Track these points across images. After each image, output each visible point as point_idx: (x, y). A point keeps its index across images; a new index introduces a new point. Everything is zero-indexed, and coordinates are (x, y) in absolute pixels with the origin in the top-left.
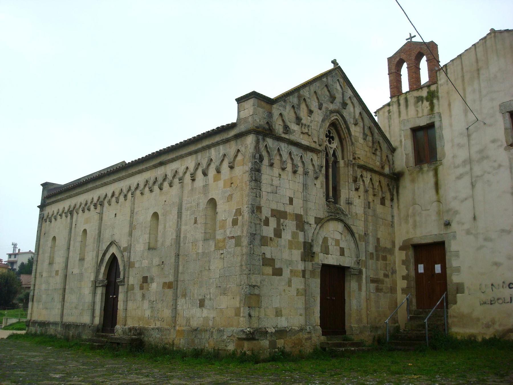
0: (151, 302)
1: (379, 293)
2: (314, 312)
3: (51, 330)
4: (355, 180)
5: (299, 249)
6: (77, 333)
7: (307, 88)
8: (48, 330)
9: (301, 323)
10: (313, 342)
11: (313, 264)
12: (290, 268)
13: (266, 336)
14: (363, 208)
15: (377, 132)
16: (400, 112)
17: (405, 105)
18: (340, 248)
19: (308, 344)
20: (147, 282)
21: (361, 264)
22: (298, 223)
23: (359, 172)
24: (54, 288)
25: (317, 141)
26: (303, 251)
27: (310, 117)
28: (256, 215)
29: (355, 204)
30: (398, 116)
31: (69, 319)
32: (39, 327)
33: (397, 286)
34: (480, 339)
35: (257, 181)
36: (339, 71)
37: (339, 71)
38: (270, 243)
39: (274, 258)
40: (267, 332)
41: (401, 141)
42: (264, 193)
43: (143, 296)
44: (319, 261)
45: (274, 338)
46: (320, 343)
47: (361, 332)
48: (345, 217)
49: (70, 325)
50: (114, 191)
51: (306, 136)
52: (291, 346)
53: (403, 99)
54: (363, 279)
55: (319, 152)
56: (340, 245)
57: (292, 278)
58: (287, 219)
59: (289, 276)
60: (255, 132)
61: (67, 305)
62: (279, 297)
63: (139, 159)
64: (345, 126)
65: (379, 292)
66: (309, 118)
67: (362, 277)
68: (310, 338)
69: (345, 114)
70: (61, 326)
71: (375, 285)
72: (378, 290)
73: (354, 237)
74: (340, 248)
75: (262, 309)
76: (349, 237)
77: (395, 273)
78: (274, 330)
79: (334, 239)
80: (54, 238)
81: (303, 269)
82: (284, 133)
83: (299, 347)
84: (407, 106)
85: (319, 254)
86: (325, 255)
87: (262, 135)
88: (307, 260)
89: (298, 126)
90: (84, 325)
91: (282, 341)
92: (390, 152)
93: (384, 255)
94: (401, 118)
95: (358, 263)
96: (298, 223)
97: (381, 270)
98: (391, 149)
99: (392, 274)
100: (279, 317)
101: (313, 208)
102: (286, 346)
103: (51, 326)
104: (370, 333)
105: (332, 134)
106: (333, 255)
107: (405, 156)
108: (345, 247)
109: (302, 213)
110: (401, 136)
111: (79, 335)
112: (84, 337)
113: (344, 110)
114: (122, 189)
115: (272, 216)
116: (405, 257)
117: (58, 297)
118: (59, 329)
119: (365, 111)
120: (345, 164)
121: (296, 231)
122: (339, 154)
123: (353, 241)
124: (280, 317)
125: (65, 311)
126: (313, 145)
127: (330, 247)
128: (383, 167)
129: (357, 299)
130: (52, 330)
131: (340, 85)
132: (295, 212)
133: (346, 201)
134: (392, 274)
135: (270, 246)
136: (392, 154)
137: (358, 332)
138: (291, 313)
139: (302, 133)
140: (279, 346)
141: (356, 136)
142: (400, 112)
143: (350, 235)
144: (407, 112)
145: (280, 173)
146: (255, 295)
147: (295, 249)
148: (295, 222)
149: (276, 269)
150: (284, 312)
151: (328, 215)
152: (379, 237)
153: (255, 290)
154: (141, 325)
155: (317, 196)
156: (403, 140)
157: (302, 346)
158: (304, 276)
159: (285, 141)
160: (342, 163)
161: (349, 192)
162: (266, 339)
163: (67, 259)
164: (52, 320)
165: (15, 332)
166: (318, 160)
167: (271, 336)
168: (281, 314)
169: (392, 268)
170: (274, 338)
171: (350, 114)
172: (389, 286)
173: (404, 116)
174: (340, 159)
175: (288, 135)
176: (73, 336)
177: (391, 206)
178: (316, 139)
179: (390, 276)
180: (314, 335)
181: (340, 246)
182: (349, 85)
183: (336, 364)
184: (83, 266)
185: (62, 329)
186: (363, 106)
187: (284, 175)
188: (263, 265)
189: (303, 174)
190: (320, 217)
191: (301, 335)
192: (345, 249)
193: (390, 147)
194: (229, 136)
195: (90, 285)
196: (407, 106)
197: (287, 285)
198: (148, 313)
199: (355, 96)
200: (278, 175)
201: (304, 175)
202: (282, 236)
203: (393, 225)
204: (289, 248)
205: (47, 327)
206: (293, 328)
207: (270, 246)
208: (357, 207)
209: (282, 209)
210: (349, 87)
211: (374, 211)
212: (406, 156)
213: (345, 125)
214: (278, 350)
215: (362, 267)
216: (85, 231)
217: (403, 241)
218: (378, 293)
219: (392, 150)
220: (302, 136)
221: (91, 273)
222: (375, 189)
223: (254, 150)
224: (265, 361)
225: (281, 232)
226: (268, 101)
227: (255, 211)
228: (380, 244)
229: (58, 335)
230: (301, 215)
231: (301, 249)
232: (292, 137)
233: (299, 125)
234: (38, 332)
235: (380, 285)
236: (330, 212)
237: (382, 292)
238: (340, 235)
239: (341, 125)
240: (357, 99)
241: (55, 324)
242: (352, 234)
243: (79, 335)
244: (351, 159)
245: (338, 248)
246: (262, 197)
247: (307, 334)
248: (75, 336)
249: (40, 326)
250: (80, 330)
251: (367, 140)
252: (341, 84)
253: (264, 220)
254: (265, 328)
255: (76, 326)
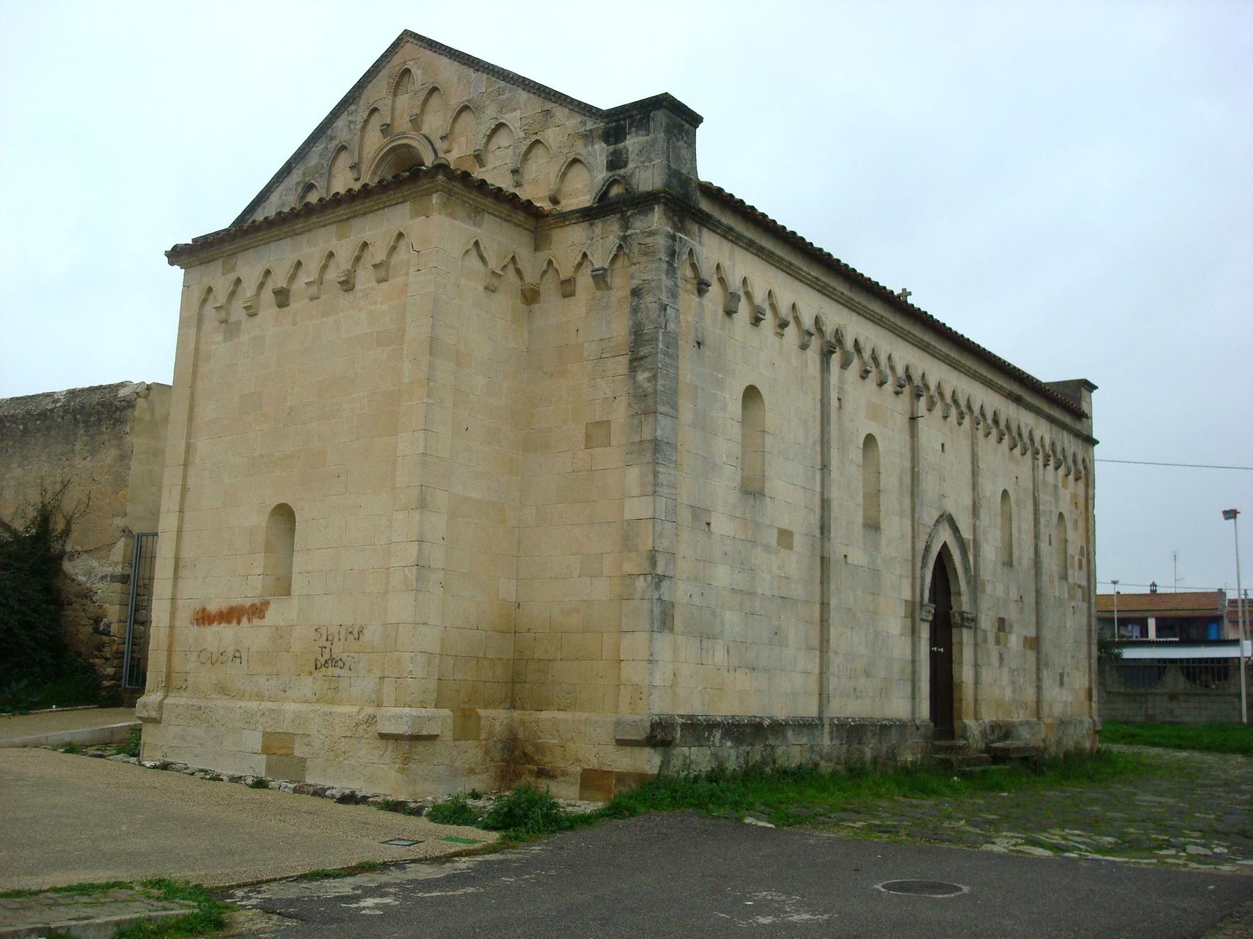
0: (1011, 671)
3: (792, 752)
6: (884, 749)
8: (779, 751)
20: (1004, 631)
24: (776, 593)
31: (848, 708)
32: (729, 744)
34: (767, 722)
43: (1001, 658)
49: (864, 725)
50: (856, 340)
61: (836, 661)
63: (846, 265)
70: (831, 733)
80: (751, 394)
90: (902, 726)
103: (790, 734)
111: (892, 755)
112: (908, 757)
114: (924, 374)
117: (797, 630)
118: (826, 741)
125: (833, 682)
130: (796, 751)
154: (1001, 718)
163: (825, 504)
164: (780, 713)
176: (875, 760)
183: (892, 772)
184: (876, 547)
185: (837, 742)
194: (757, 241)
195: (901, 611)
198: (1008, 693)
205: (771, 742)
216: (870, 439)
221: (901, 576)
229: (823, 764)
234: (732, 765)
241: (806, 726)
243: (892, 755)
248: (880, 757)
249: (738, 741)
250: (894, 737)
255: (884, 728)
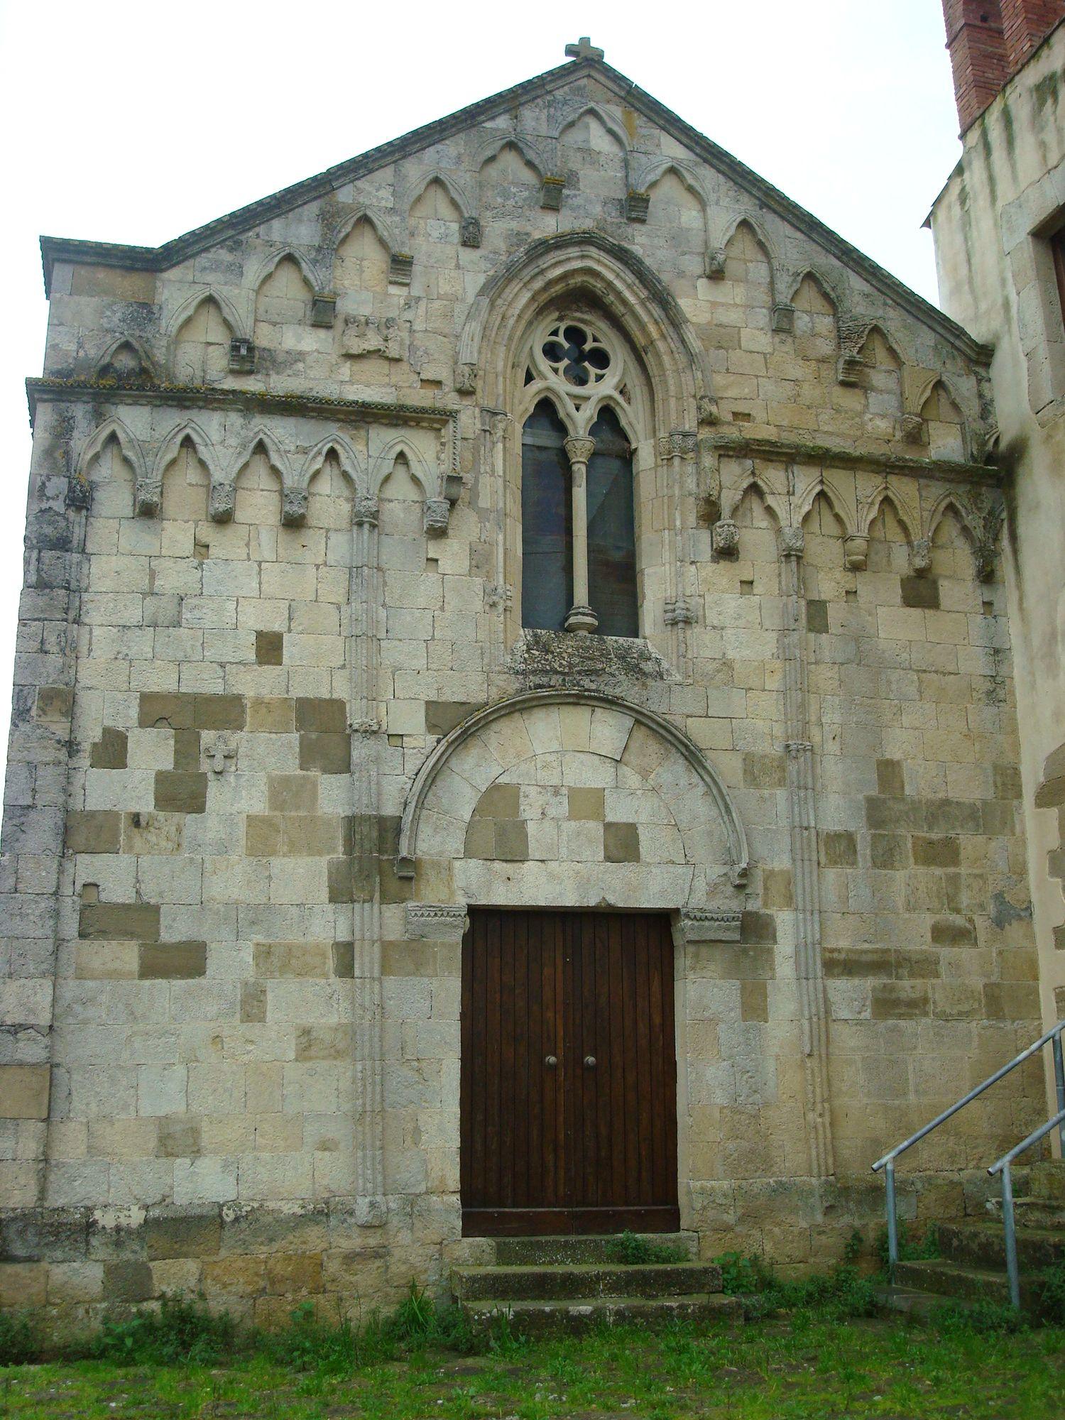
1: (902, 1023)
2: (417, 1131)
4: (710, 513)
5: (313, 851)
7: (386, 174)
9: (325, 1182)
10: (397, 1268)
11: (406, 911)
12: (259, 938)
13: (87, 1243)
14: (774, 635)
15: (866, 288)
16: (991, 180)
17: (1004, 145)
18: (608, 826)
19: (366, 1277)
21: (761, 891)
22: (314, 736)
23: (734, 477)
25: (443, 373)
26: (342, 857)
27: (407, 285)
28: (38, 727)
29: (712, 618)
30: (988, 204)
33: (1036, 978)
35: (52, 588)
36: (593, 73)
37: (593, 73)
38: (129, 838)
39: (153, 901)
40: (89, 1227)
41: (1006, 305)
42: (97, 632)
44: (452, 893)
45: (134, 1252)
46: (446, 1273)
47: (752, 1217)
48: (644, 684)
51: (373, 367)
52: (250, 1289)
53: (997, 120)
54: (778, 959)
55: (447, 421)
56: (607, 811)
57: (270, 984)
58: (240, 728)
59: (250, 974)
60: (44, 392)
62: (180, 1070)
64: (644, 294)
65: (900, 1016)
66: (393, 290)
67: (770, 952)
68: (380, 1253)
69: (640, 242)
71: (869, 983)
72: (887, 1005)
73: (703, 773)
74: (608, 826)
75: (72, 1125)
76: (674, 771)
77: (1020, 918)
78: (136, 1217)
79: (564, 791)
81: (343, 936)
82: (233, 372)
83: (304, 1292)
84: (1010, 142)
85: (457, 864)
86: (497, 865)
87: (85, 399)
88: (358, 895)
89: (322, 333)
91: (190, 1267)
92: (960, 362)
93: (935, 835)
94: (1000, 204)
95: (740, 887)
96: (314, 736)
97: (910, 908)
98: (968, 351)
99: (1000, 922)
100: (179, 1161)
101: (420, 663)
102: (211, 1288)
104: (819, 1218)
105: (595, 340)
106: (553, 865)
107: (1024, 363)
108: (642, 818)
109: (341, 692)
110: (1003, 282)
113: (637, 226)
115: (146, 721)
116: (1057, 834)
119: (775, 212)
120: (657, 453)
121: (299, 772)
122: (633, 417)
123: (701, 789)
124: (188, 1161)
126: (420, 398)
127: (531, 828)
128: (915, 438)
129: (730, 1057)
131: (611, 132)
132: (297, 693)
133: (666, 612)
134: (1000, 922)
135: (130, 849)
136: (976, 373)
137: (730, 1218)
138: (260, 1140)
139: (349, 356)
140: (164, 1288)
141: (720, 325)
142: (991, 180)
143: (681, 761)
144: (1013, 167)
145: (204, 540)
146: (21, 1065)
147: (293, 849)
148: (295, 737)
149: (166, 947)
150: (208, 1136)
151: (517, 685)
152: (894, 753)
153: (21, 1044)
155: (442, 609)
156: (1013, 297)
157: (319, 1289)
158: (346, 969)
159: (219, 401)
160: (645, 457)
161: (680, 574)
162: (87, 1253)
165: (531, 1305)
166: (443, 456)
167: (118, 1244)
168: (195, 1143)
169: (999, 897)
170: (133, 1253)
171: (677, 238)
172: (977, 983)
173: (1006, 192)
174: (641, 437)
175: (259, 377)
177: (988, 604)
178: (438, 371)
179: (982, 936)
180: (405, 1237)
181: (610, 818)
182: (662, 122)
186: (758, 194)
187: (224, 544)
188: (83, 935)
189: (352, 524)
190: (464, 700)
191: (314, 1238)
192: (641, 830)
193: (958, 343)
196: (1010, 142)
197: (238, 1016)
199: (705, 161)
200: (189, 547)
201: (355, 528)
202: (208, 804)
203: (1001, 694)
204: (252, 852)
206: (271, 1205)
207: (130, 849)
208: (729, 633)
209: (216, 688)
210: (663, 129)
211: (859, 640)
212: (1029, 360)
213: (646, 287)
214: (165, 1305)
215: (765, 905)
217: (1048, 758)
218: (890, 1022)
219: (973, 356)
220: (346, 369)
222: (852, 538)
223: (40, 466)
224: (73, 1355)
225: (206, 787)
226: (128, 263)
227: (34, 712)
228: (907, 787)
230: (339, 705)
231: (332, 850)
232: (280, 384)
233: (329, 327)
235: (906, 983)
236: (534, 672)
237: (926, 1014)
238: (609, 768)
239: (618, 294)
240: (719, 171)
242: (692, 756)
244: (690, 424)
245: (596, 829)
246: (84, 649)
247: (356, 1230)
251: (798, 333)
252: (611, 125)
253: (95, 745)
254: (89, 1210)
